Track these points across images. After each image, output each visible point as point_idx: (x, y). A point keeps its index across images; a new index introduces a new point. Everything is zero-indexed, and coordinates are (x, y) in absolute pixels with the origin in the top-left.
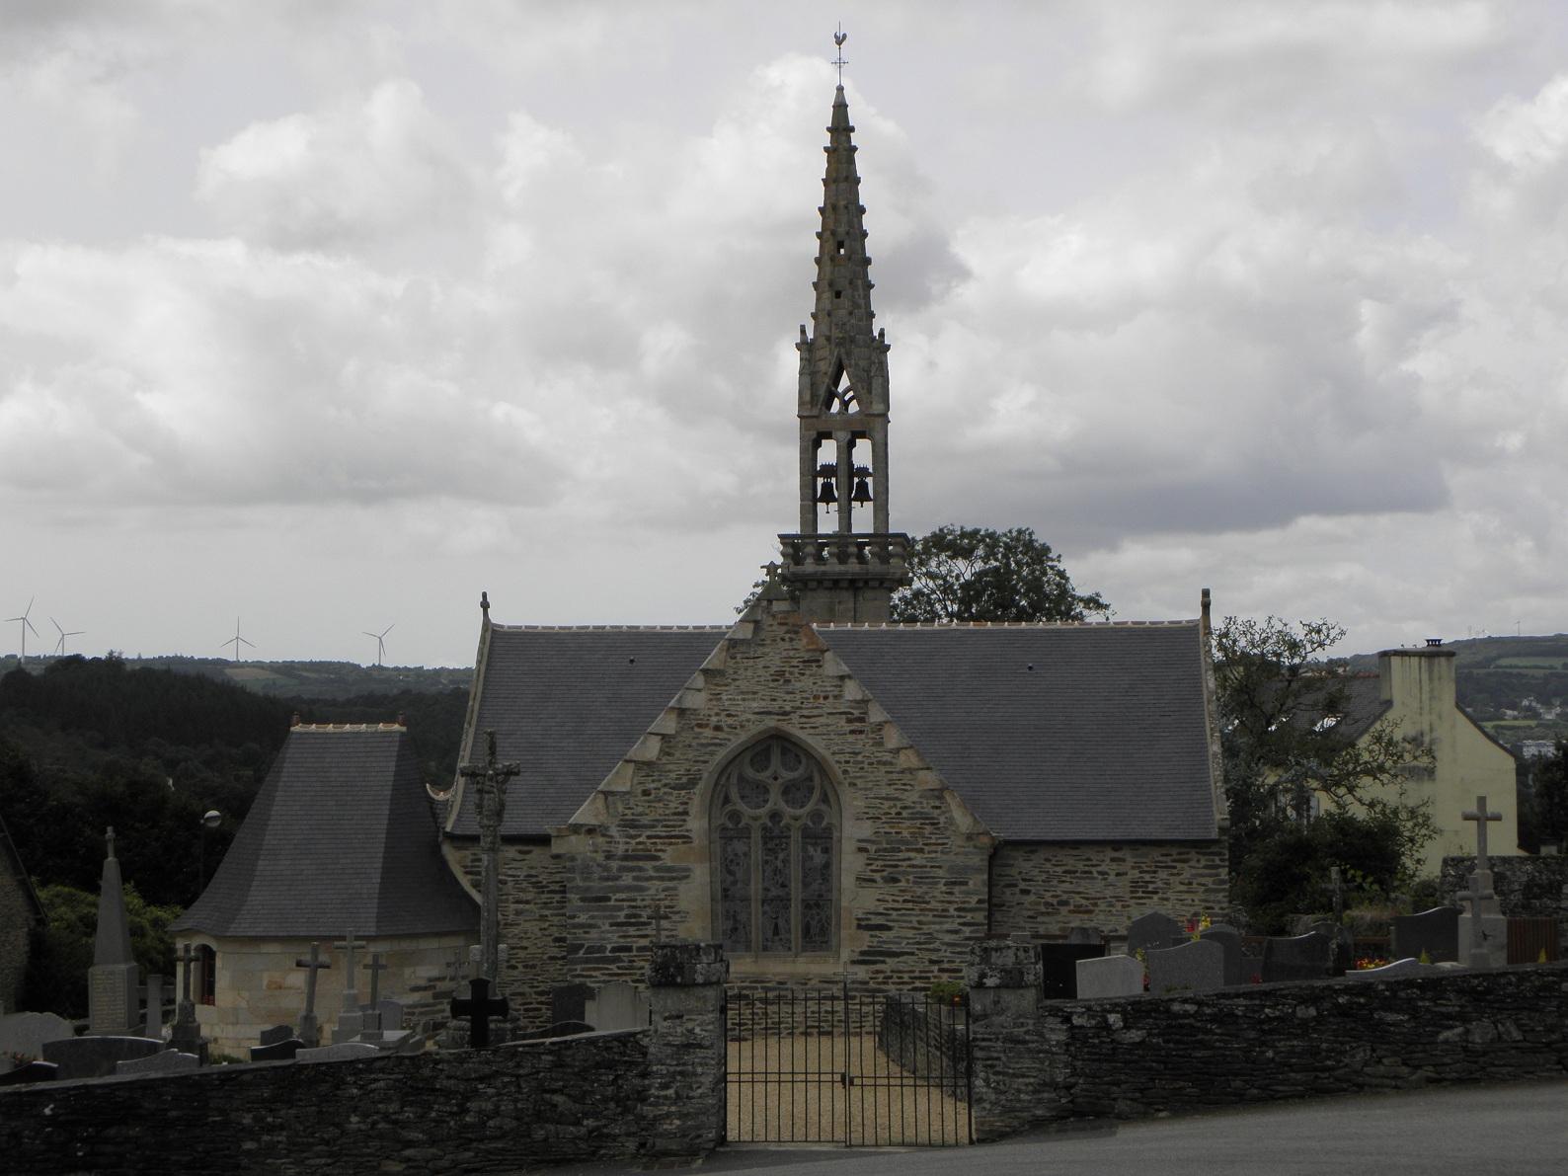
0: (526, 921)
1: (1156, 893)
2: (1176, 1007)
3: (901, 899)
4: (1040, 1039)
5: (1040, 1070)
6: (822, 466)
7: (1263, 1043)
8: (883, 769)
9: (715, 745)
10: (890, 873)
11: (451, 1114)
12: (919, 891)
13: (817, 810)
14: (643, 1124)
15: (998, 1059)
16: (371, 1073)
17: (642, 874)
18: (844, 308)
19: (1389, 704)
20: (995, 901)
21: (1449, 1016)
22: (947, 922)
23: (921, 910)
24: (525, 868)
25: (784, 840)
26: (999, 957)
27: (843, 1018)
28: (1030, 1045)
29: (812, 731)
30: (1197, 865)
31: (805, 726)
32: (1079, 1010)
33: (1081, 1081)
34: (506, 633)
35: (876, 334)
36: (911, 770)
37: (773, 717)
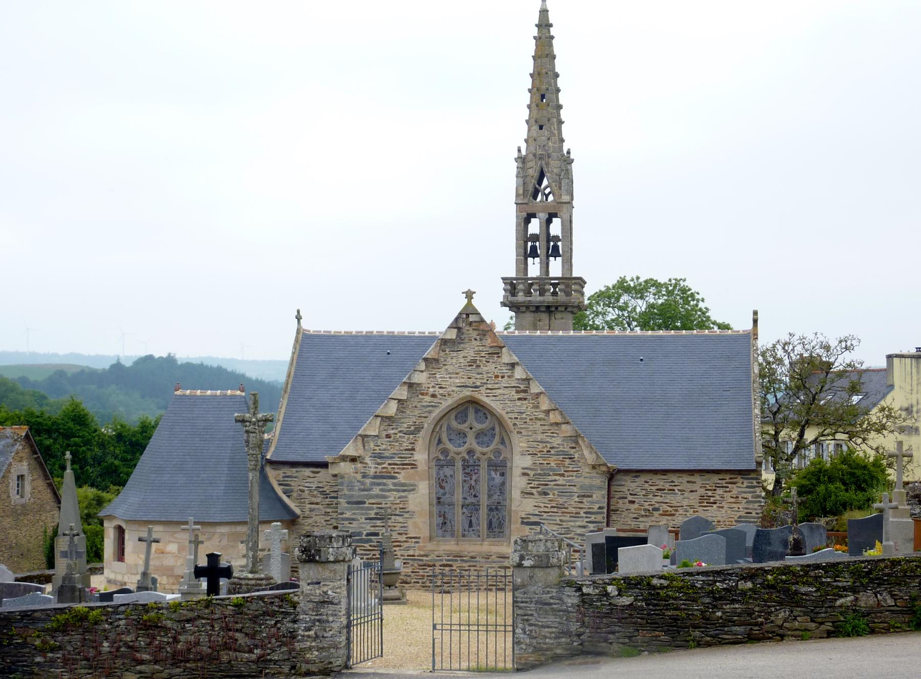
0: (316, 515)
1: (715, 503)
2: (655, 582)
3: (549, 506)
4: (561, 602)
5: (560, 623)
6: (530, 235)
7: (715, 607)
8: (539, 423)
9: (432, 406)
10: (543, 489)
11: (168, 643)
12: (561, 501)
13: (497, 448)
14: (293, 654)
15: (532, 615)
16: (117, 615)
17: (385, 487)
18: (544, 136)
19: (891, 387)
20: (612, 507)
21: (844, 589)
22: (578, 521)
23: (562, 513)
24: (316, 482)
25: (476, 467)
26: (534, 546)
27: (512, 580)
28: (554, 606)
29: (494, 398)
30: (742, 486)
31: (489, 395)
32: (588, 583)
33: (587, 631)
34: (311, 335)
35: (565, 152)
36: (557, 424)
37: (469, 389)
